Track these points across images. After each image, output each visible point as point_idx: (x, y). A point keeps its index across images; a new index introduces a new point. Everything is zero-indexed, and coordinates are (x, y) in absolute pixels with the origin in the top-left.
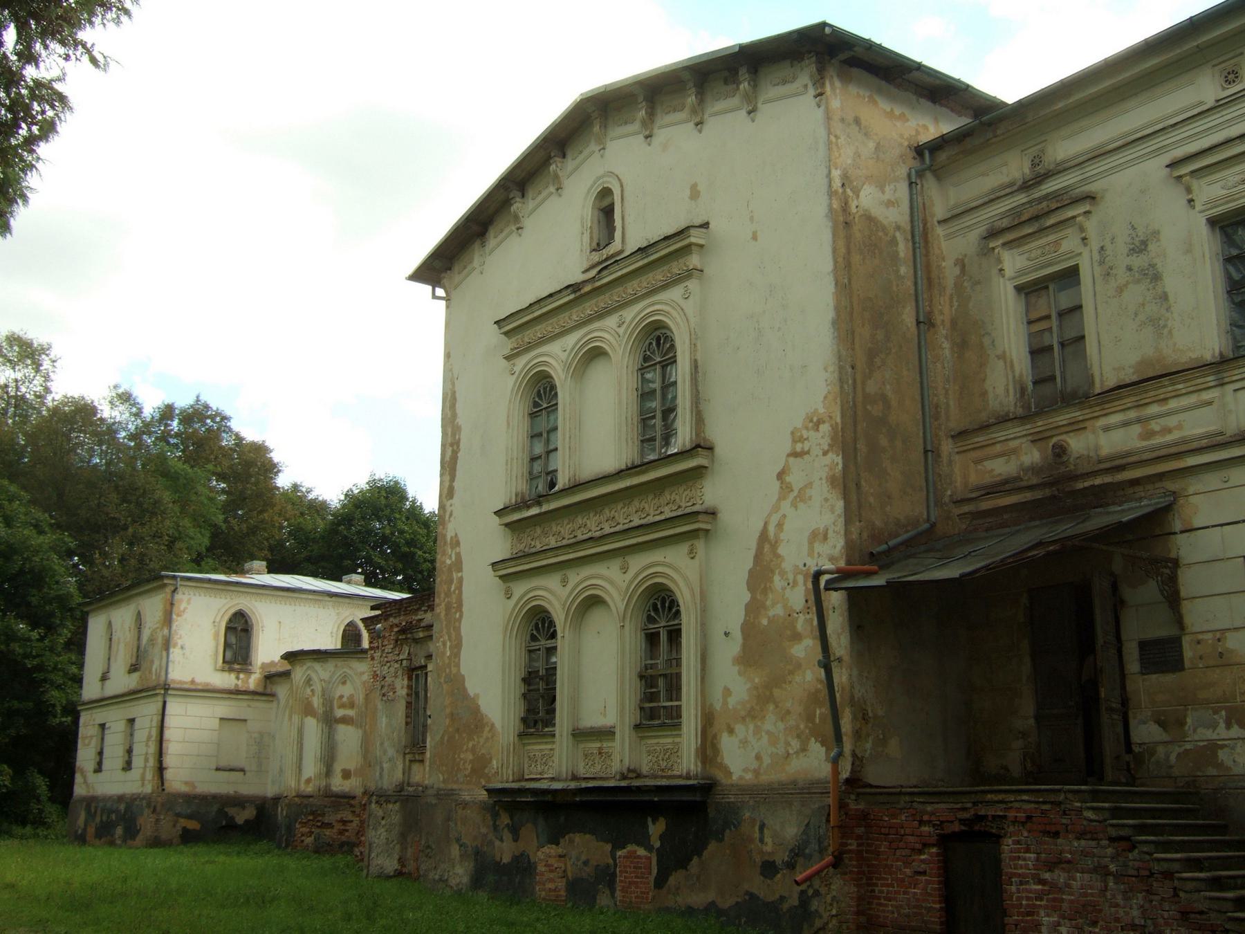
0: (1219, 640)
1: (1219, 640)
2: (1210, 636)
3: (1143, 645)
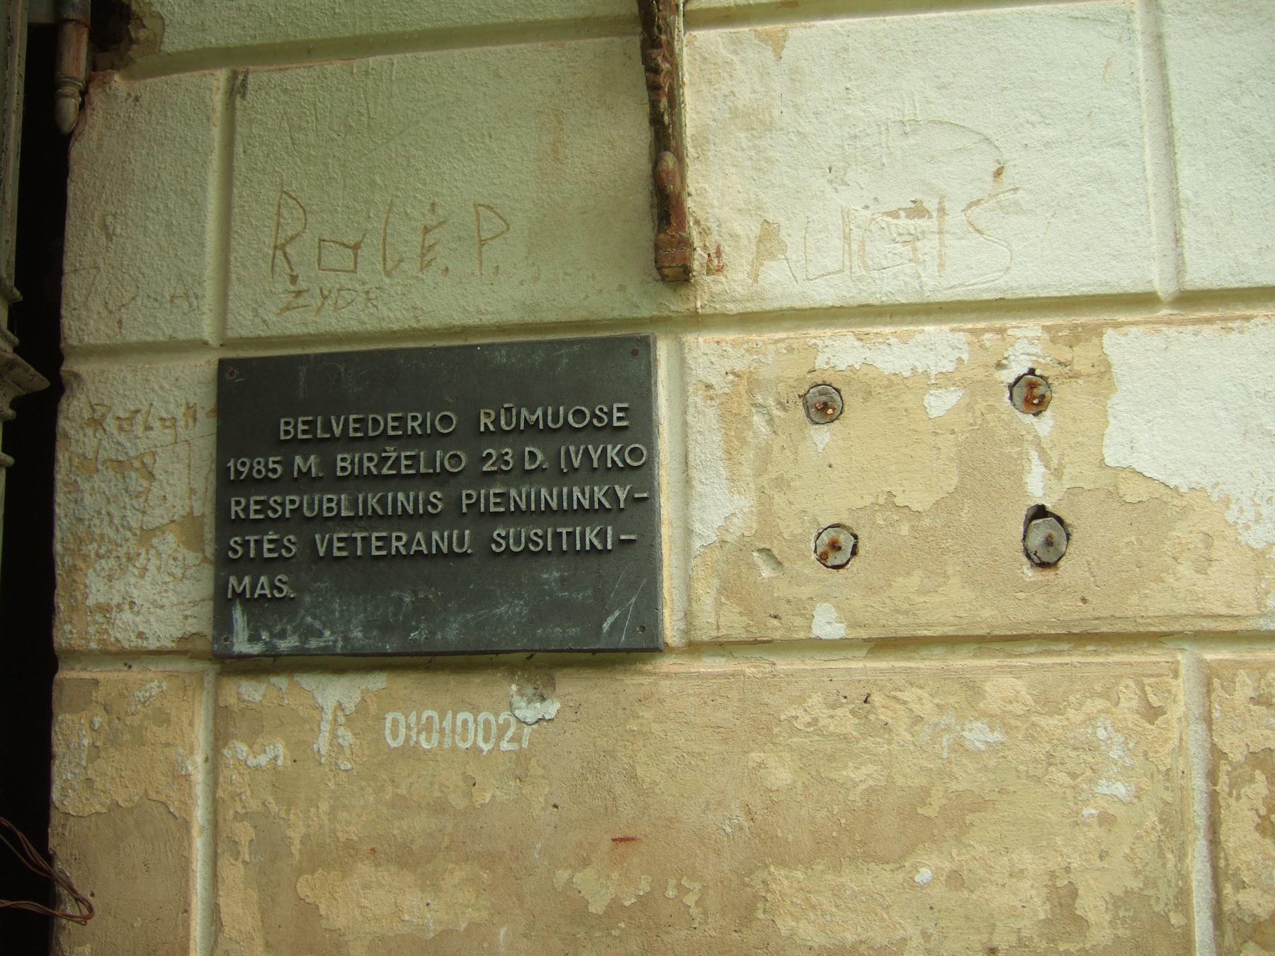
0: (1032, 393)
1: (1032, 393)
2: (938, 346)
3: (262, 400)
